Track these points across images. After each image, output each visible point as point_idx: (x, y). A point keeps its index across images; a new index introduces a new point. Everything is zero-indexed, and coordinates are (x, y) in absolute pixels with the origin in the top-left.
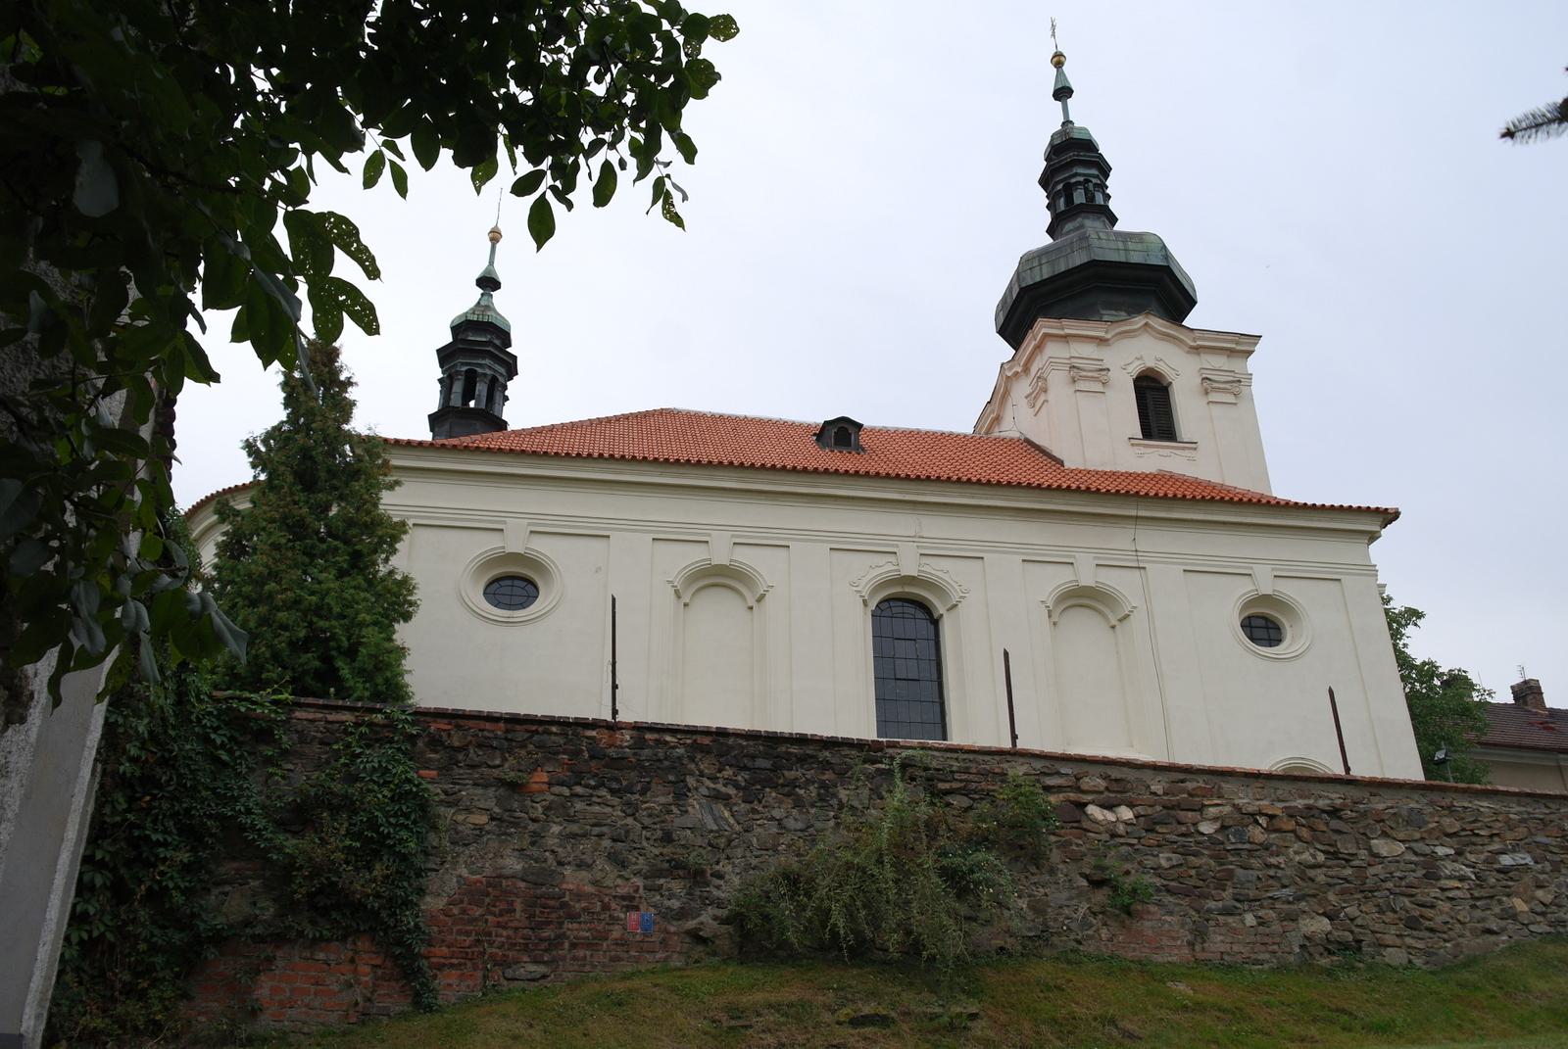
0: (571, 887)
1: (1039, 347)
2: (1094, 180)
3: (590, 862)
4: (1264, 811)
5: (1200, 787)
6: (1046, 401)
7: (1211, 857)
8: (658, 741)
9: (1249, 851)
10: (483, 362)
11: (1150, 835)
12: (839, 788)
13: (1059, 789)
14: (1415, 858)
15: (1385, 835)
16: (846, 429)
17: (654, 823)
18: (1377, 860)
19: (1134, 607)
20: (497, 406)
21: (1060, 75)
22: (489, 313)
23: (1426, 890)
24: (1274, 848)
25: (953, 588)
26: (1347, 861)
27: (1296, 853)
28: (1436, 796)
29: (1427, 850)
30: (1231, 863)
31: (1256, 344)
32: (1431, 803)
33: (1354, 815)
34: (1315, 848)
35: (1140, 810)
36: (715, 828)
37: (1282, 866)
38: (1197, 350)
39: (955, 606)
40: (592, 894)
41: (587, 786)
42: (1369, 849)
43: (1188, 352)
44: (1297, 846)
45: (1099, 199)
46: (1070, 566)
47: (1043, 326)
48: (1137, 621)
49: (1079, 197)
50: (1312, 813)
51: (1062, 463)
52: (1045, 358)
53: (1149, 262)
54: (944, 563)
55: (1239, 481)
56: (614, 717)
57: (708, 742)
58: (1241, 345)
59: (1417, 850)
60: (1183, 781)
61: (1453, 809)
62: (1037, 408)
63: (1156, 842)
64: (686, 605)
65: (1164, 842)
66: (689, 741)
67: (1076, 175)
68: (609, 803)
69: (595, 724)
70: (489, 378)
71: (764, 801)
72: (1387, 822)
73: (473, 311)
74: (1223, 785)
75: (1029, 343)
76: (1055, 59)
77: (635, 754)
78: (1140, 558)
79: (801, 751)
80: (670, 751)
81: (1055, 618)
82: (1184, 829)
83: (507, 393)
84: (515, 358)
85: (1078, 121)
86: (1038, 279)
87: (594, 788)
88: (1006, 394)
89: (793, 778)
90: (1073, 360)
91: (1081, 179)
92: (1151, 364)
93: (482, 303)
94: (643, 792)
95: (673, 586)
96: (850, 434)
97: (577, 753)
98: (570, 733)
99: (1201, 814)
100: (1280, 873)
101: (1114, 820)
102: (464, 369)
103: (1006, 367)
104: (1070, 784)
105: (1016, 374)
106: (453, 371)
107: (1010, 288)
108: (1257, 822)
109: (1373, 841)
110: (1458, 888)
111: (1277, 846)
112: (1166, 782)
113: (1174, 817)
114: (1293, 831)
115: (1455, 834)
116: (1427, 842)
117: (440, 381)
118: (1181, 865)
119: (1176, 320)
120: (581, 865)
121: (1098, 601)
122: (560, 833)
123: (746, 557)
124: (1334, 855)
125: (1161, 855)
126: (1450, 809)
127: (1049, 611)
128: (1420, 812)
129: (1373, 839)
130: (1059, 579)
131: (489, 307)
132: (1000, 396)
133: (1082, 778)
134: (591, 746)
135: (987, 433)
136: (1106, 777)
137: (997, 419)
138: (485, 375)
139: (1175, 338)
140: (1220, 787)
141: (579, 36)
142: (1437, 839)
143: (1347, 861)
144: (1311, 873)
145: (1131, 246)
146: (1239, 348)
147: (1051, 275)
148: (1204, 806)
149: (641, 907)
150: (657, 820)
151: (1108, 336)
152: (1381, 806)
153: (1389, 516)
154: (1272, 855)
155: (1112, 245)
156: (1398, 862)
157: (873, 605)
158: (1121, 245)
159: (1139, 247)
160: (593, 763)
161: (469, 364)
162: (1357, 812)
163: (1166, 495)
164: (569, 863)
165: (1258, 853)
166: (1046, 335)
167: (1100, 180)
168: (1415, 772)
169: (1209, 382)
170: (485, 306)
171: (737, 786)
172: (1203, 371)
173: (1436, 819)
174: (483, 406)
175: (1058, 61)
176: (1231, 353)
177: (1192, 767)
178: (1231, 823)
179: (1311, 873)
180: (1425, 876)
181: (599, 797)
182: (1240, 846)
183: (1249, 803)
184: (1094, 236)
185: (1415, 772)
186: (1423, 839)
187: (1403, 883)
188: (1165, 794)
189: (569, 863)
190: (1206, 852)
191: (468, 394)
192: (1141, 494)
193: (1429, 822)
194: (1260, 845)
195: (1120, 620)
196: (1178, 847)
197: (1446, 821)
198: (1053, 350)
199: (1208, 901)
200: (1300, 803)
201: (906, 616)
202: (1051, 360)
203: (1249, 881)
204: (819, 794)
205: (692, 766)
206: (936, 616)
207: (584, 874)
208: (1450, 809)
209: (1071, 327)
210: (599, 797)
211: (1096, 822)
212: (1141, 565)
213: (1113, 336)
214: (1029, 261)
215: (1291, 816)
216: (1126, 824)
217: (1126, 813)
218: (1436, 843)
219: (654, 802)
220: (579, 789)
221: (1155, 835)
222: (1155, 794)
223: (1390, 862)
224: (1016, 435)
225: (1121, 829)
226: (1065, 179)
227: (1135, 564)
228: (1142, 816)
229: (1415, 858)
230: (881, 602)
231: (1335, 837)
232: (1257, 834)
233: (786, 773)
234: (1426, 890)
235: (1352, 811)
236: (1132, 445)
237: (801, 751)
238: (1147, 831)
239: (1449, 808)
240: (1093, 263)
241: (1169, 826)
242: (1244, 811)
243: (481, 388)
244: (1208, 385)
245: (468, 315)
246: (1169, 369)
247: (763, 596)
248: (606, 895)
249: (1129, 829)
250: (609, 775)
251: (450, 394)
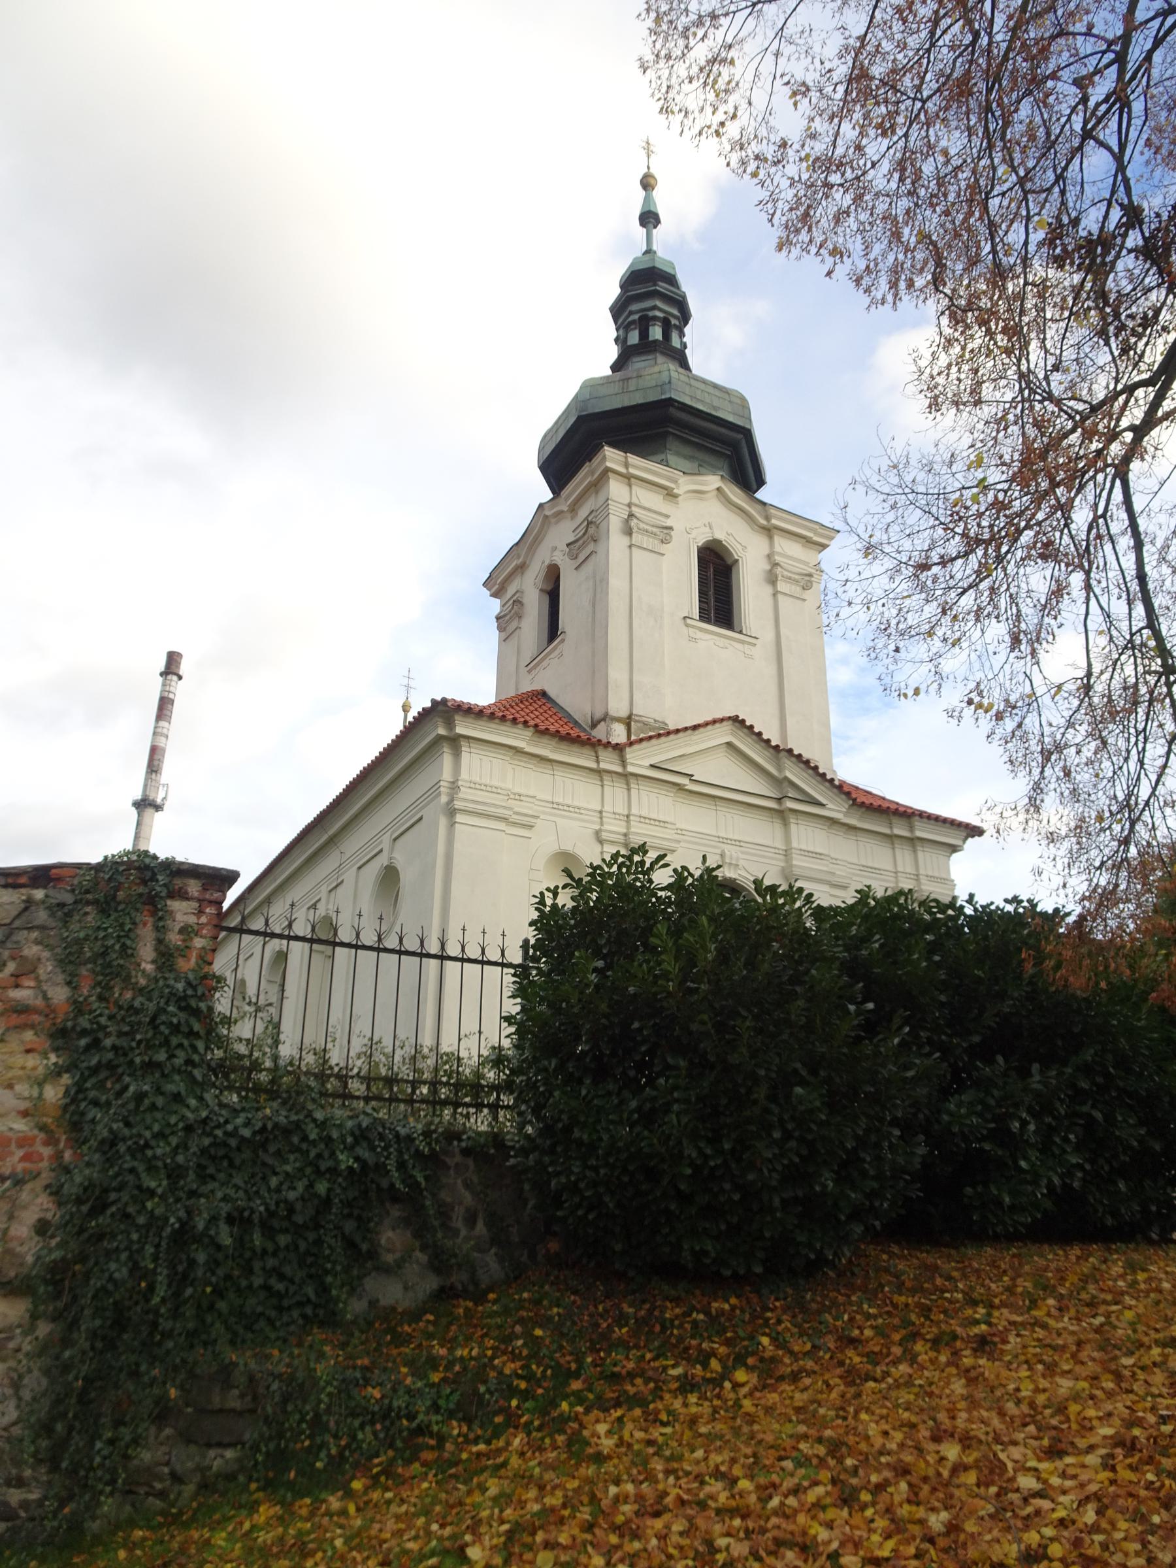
45: (676, 342)
49: (656, 333)
62: (582, 557)
67: (655, 308)
92: (720, 536)
141: (486, 1224)
175: (647, 183)
176: (808, 541)
214: (591, 387)
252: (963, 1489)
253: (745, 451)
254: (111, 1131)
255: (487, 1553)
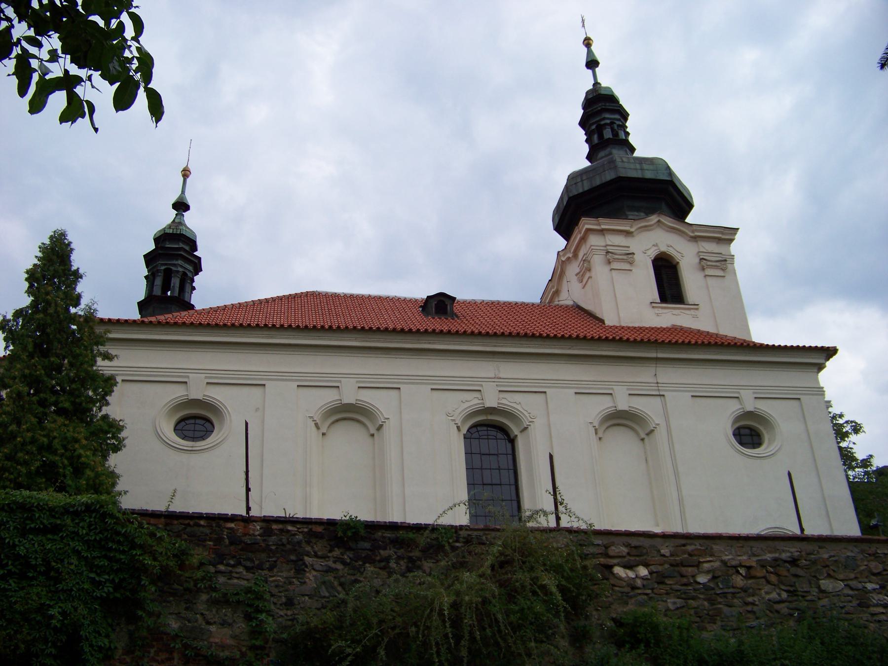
0: (217, 640)
1: (583, 239)
2: (618, 123)
3: (230, 621)
4: (743, 564)
5: (697, 549)
6: (590, 277)
7: (705, 599)
8: (281, 530)
9: (733, 593)
10: (176, 263)
11: (661, 586)
12: (423, 562)
13: (594, 556)
14: (851, 592)
15: (829, 576)
16: (443, 302)
17: (280, 592)
18: (824, 595)
19: (658, 424)
20: (187, 295)
21: (590, 53)
22: (181, 227)
23: (860, 616)
24: (751, 591)
25: (526, 417)
26: (803, 597)
27: (767, 593)
28: (865, 546)
29: (860, 586)
30: (720, 603)
31: (736, 234)
32: (862, 552)
33: (808, 563)
34: (781, 589)
35: (653, 568)
36: (327, 594)
37: (757, 603)
38: (695, 239)
39: (526, 428)
40: (232, 645)
41: (228, 565)
42: (819, 587)
43: (689, 241)
44: (768, 588)
46: (610, 396)
47: (586, 223)
48: (661, 434)
49: (608, 134)
50: (778, 563)
51: (602, 321)
52: (588, 247)
53: (658, 178)
54: (517, 397)
55: (727, 330)
56: (248, 513)
57: (320, 530)
58: (726, 235)
59: (852, 586)
60: (684, 545)
61: (877, 555)
63: (665, 592)
64: (324, 434)
65: (671, 591)
66: (306, 530)
67: (604, 119)
68: (245, 578)
69: (234, 518)
70: (180, 274)
71: (365, 573)
72: (831, 567)
73: (170, 226)
74: (714, 547)
75: (577, 236)
76: (586, 42)
77: (264, 540)
78: (660, 388)
79: (393, 535)
80: (292, 537)
81: (600, 434)
82: (685, 580)
83: (194, 284)
84: (199, 259)
85: (604, 82)
86: (581, 191)
87: (233, 566)
88: (562, 273)
89: (387, 555)
90: (608, 248)
91: (608, 121)
92: (663, 249)
93: (176, 221)
94: (271, 569)
95: (314, 421)
96: (447, 305)
97: (219, 540)
98: (214, 525)
99: (698, 569)
100: (755, 609)
101: (633, 576)
102: (163, 268)
103: (561, 254)
104: (600, 552)
105: (569, 258)
106: (155, 270)
107: (561, 198)
108: (738, 572)
109: (821, 582)
110: (883, 613)
111: (753, 589)
112: (673, 547)
113: (679, 572)
114: (764, 577)
115: (879, 574)
116: (860, 580)
117: (146, 277)
118: (683, 607)
119: (681, 218)
120: (224, 624)
121: (631, 420)
122: (208, 600)
123: (368, 398)
124: (792, 593)
125: (669, 601)
126: (875, 555)
127: (596, 430)
128: (854, 558)
129: (821, 579)
130: (603, 405)
131: (181, 223)
132: (558, 275)
133: (609, 547)
134: (229, 535)
135: (549, 303)
136: (627, 545)
137: (557, 293)
138: (178, 272)
139: (679, 230)
140: (712, 548)
142: (867, 577)
143: (803, 597)
144: (777, 607)
145: (645, 167)
146: (724, 237)
147: (590, 187)
148: (700, 562)
149: (271, 654)
150: (281, 589)
151: (632, 230)
152: (826, 556)
153: (830, 352)
154: (749, 596)
155: (632, 166)
156: (838, 595)
157: (464, 430)
158: (638, 166)
159: (651, 167)
160: (232, 548)
161: (166, 264)
162: (810, 561)
163: (690, 342)
164: (215, 623)
165: (738, 595)
166: (588, 230)
167: (622, 122)
168: (854, 530)
169: (704, 261)
170: (178, 223)
171: (344, 563)
172: (700, 254)
173: (866, 563)
174: (176, 294)
175: (587, 42)
176: (719, 240)
177: (690, 534)
178: (720, 574)
179: (777, 607)
180: (859, 605)
181: (237, 573)
182: (726, 590)
183: (732, 559)
184: (618, 160)
185: (854, 530)
186: (856, 578)
187: (844, 611)
188: (672, 555)
189: (215, 623)
190: (702, 596)
191: (166, 286)
192: (666, 341)
193: (860, 566)
194: (741, 588)
195: (648, 434)
196: (681, 594)
197: (873, 565)
198: (594, 241)
199: (703, 632)
200: (768, 557)
201: (490, 437)
202: (592, 247)
203: (732, 616)
204: (407, 567)
205: (308, 548)
206: (512, 437)
207: (227, 631)
208: (875, 555)
209: (606, 224)
210: (237, 573)
211: (620, 579)
212: (661, 393)
213: (636, 230)
214: (573, 178)
215: (763, 566)
216: (643, 579)
217: (643, 571)
218: (866, 580)
219: (280, 576)
220: (222, 568)
221: (664, 586)
222: (664, 556)
223: (834, 596)
224: (570, 303)
225: (639, 583)
226: (598, 121)
227: (657, 393)
228: (654, 572)
229: (851, 592)
230: (471, 428)
231: (794, 579)
232: (739, 581)
233: (382, 552)
234: (860, 616)
235: (806, 560)
236: (653, 307)
237: (393, 535)
238: (658, 583)
239: (874, 555)
240: (620, 179)
241: (675, 579)
242: (729, 565)
243: (176, 282)
244: (703, 264)
245: (166, 230)
246: (676, 252)
247: (381, 426)
248: (244, 646)
249: (645, 582)
250: (245, 557)
251: (153, 287)
252: (709, 630)
253: (675, 194)
254: (13, 530)
255: (89, 434)
